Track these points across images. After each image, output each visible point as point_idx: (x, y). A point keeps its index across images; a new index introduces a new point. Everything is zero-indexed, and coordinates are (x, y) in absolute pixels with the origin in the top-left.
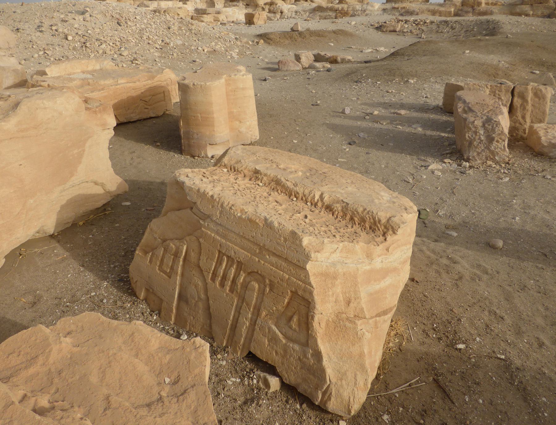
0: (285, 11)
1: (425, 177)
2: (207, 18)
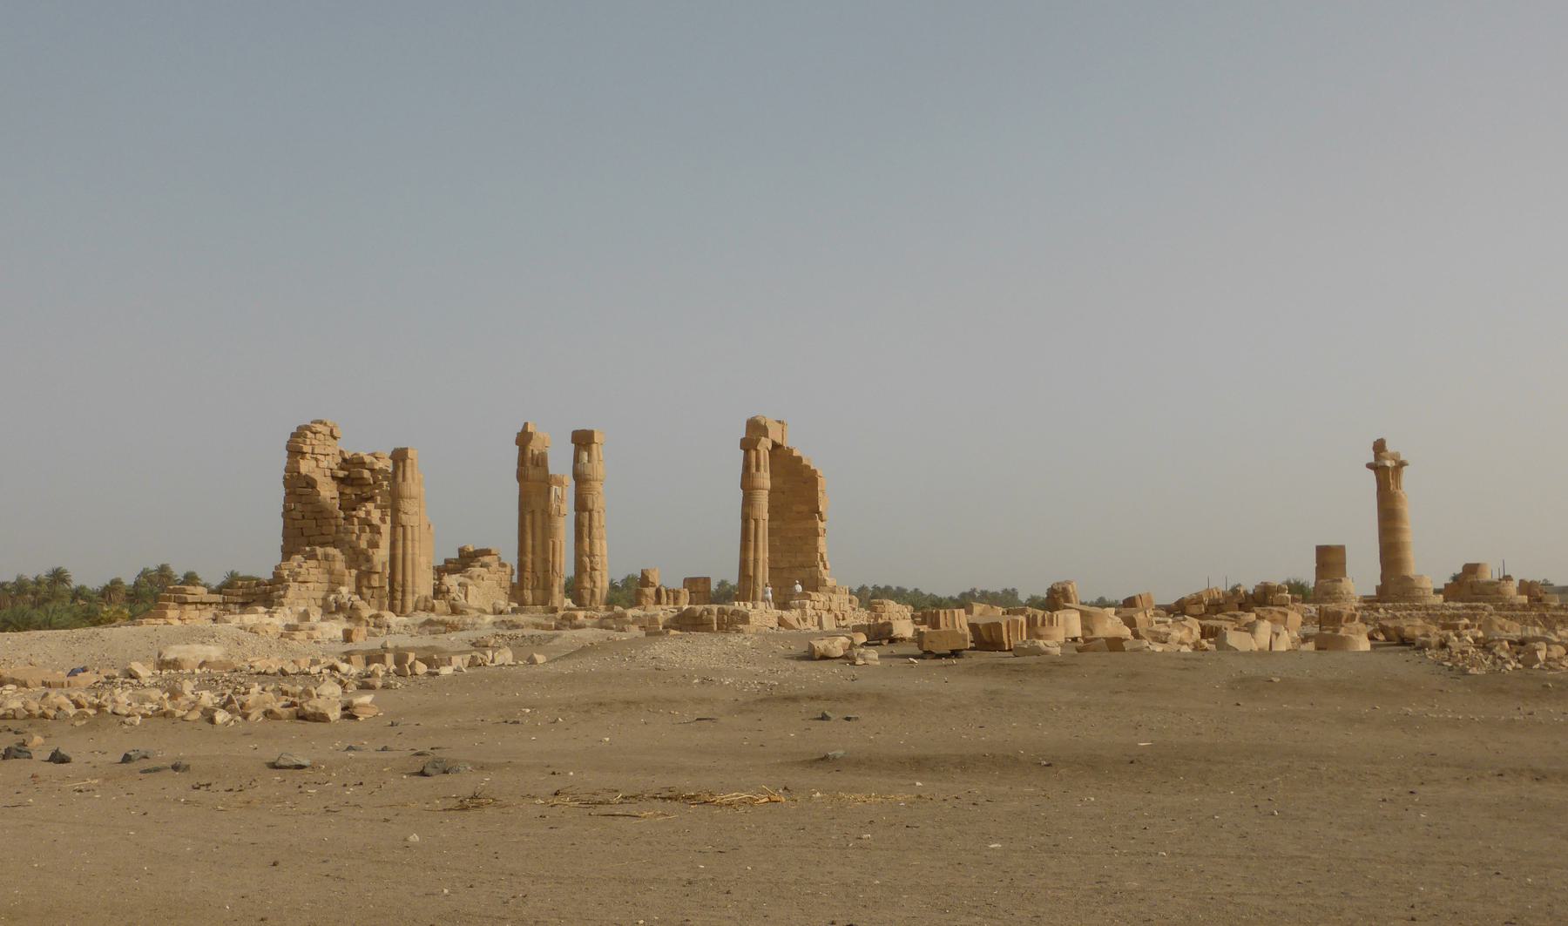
0: (393, 625)
1: (607, 739)
2: (299, 636)
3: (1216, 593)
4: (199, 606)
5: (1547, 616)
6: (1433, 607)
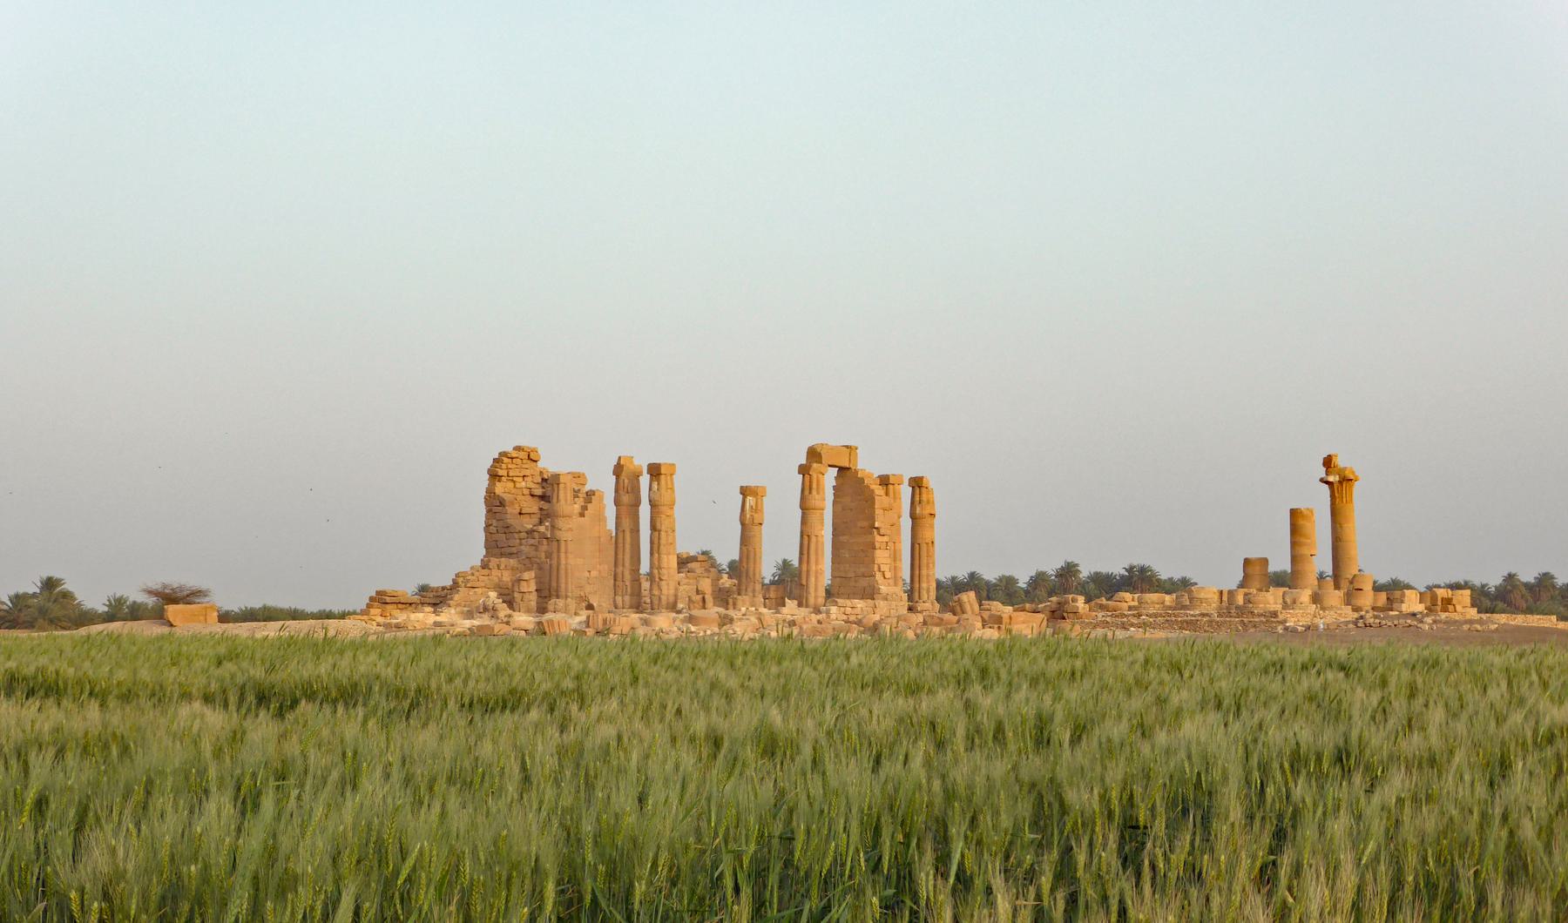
4: (400, 606)
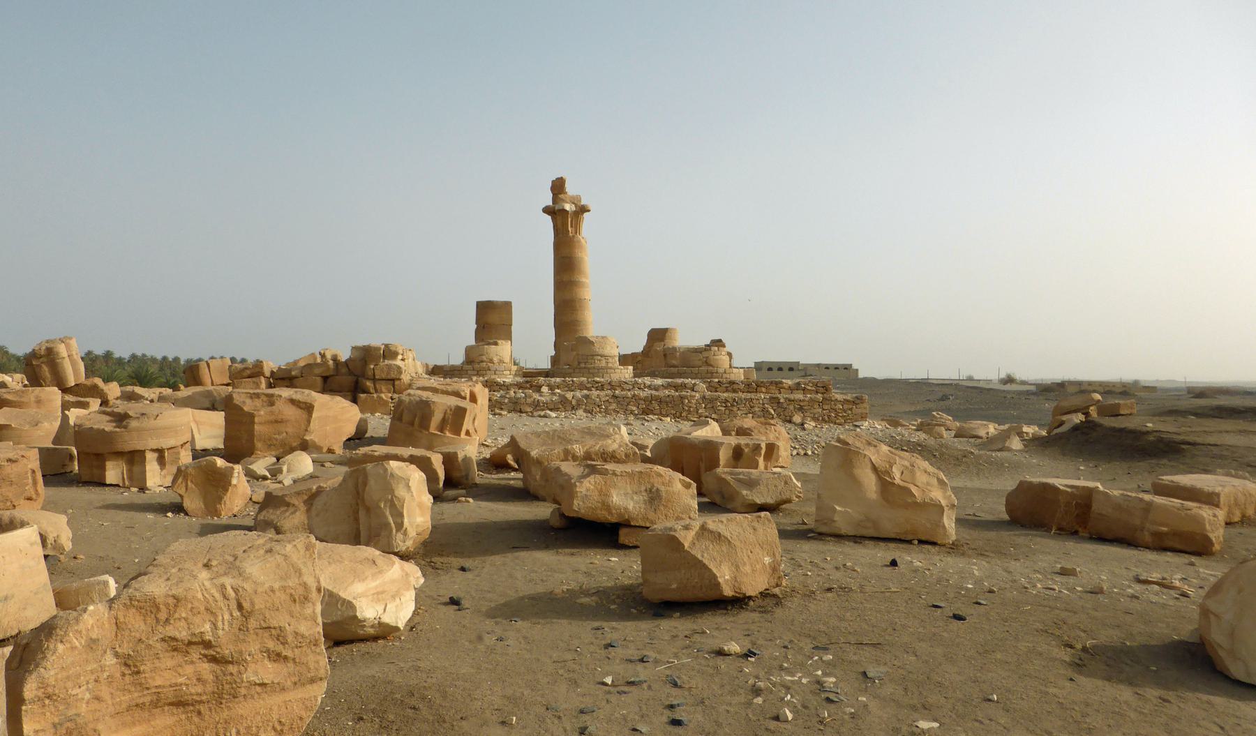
3: (318, 356)
5: (782, 401)
6: (621, 385)
